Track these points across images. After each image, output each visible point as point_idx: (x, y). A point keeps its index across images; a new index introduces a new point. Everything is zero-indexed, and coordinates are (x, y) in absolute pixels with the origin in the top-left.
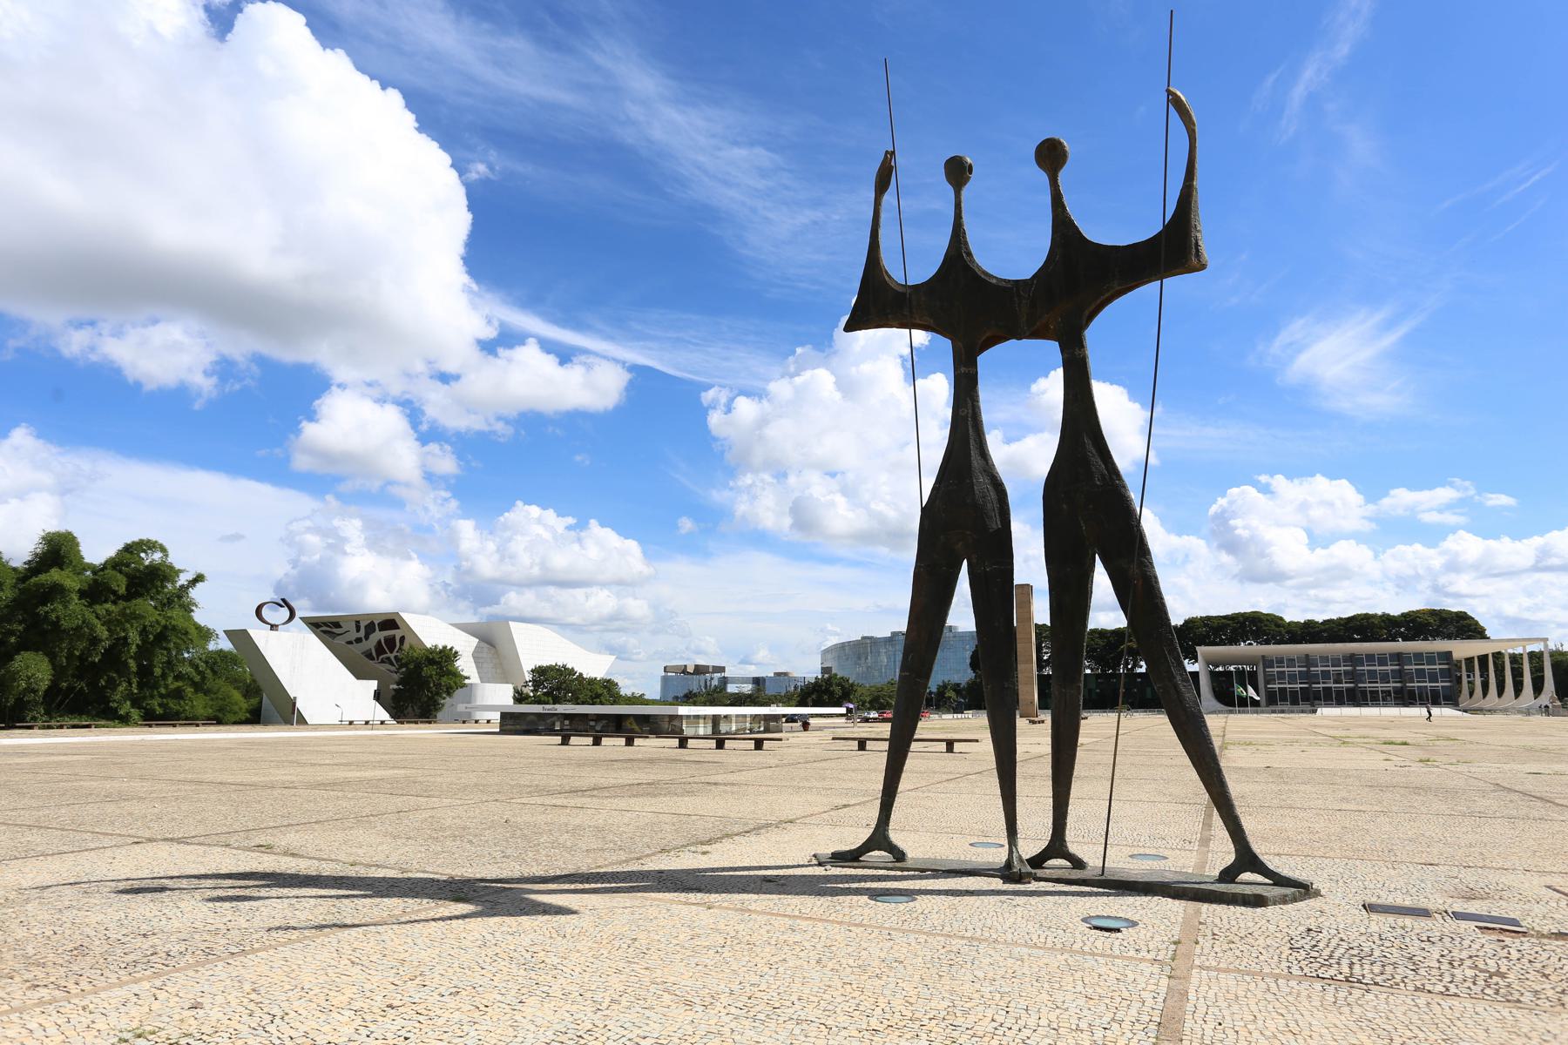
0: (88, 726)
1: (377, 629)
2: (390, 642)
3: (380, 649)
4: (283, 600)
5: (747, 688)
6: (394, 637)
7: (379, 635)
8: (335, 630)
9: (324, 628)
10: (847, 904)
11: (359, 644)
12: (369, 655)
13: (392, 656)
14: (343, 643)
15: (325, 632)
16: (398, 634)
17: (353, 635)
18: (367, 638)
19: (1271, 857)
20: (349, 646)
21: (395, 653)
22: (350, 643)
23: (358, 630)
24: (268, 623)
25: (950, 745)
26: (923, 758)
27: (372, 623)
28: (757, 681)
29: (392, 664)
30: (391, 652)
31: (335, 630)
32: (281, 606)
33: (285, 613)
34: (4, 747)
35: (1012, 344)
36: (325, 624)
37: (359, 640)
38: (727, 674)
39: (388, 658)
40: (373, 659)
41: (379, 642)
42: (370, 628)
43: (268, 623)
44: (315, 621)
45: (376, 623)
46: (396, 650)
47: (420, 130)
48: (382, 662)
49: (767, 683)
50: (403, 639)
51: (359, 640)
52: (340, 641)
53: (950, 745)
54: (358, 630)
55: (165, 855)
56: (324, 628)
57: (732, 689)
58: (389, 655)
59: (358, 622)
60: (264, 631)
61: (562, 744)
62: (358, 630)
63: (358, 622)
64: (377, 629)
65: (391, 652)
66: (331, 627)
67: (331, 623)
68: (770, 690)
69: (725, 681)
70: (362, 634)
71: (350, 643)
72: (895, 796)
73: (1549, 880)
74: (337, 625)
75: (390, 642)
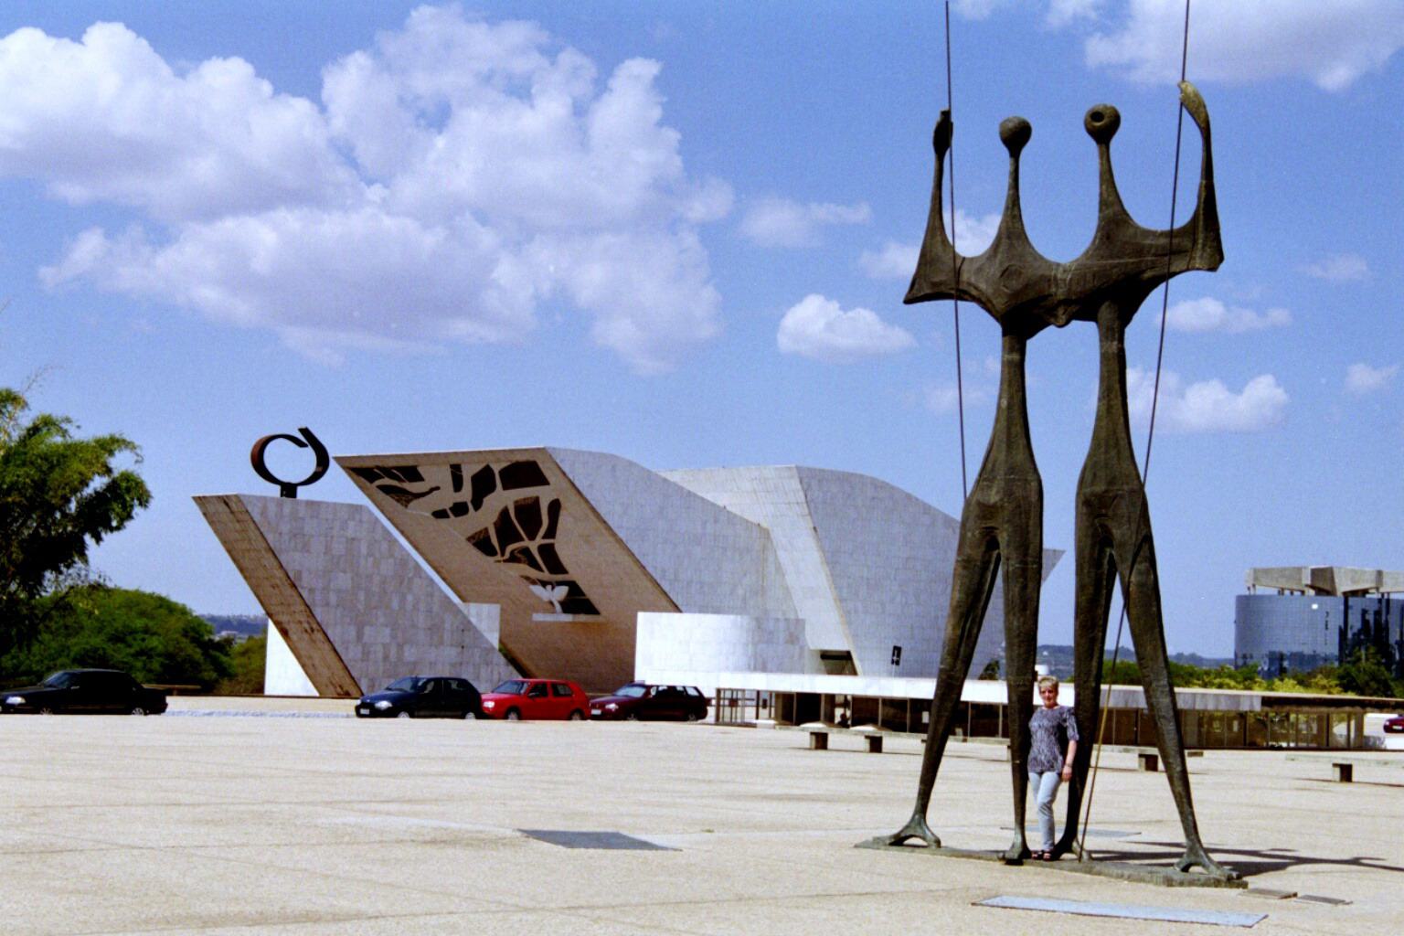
2: (528, 512)
3: (504, 527)
4: (305, 432)
6: (537, 500)
7: (503, 499)
13: (533, 546)
14: (428, 514)
15: (386, 490)
16: (545, 495)
17: (447, 498)
18: (477, 503)
21: (539, 540)
22: (440, 514)
27: (487, 471)
29: (534, 564)
33: (308, 458)
36: (387, 472)
37: (460, 509)
39: (526, 551)
41: (505, 512)
42: (484, 483)
45: (496, 468)
48: (513, 559)
50: (555, 507)
51: (460, 509)
54: (458, 485)
58: (526, 543)
65: (532, 537)
67: (397, 468)
70: (466, 494)
71: (440, 514)
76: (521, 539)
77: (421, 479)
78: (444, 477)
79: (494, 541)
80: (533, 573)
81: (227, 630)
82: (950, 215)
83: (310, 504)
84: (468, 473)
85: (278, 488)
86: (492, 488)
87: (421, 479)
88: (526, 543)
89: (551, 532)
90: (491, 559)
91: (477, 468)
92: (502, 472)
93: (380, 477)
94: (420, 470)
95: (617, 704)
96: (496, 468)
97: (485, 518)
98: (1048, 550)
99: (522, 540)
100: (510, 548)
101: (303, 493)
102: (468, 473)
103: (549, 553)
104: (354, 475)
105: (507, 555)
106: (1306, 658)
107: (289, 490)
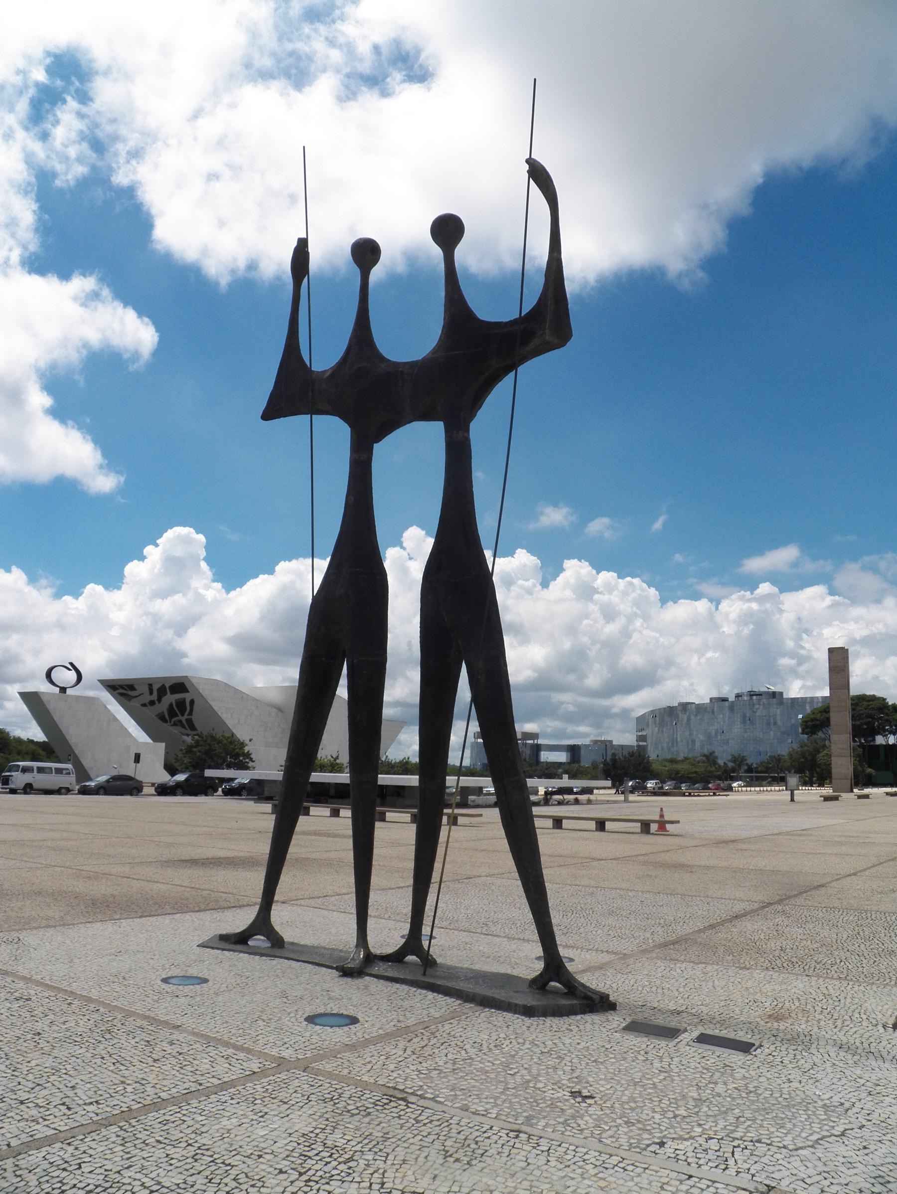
1: (168, 691)
2: (181, 704)
3: (172, 712)
4: (71, 664)
5: (562, 757)
6: (185, 699)
7: (170, 699)
10: (607, 986)
11: (152, 707)
12: (162, 718)
13: (183, 719)
14: (139, 705)
15: (122, 694)
16: (187, 697)
17: (147, 698)
18: (159, 700)
20: (144, 708)
21: (186, 717)
22: (144, 705)
24: (57, 686)
25: (645, 827)
27: (163, 687)
28: (574, 751)
29: (183, 727)
32: (70, 670)
33: (72, 675)
35: (337, 418)
36: (121, 687)
37: (152, 703)
38: (540, 741)
39: (180, 721)
40: (165, 721)
41: (171, 705)
42: (162, 691)
43: (57, 686)
44: (112, 684)
45: (167, 686)
47: (528, 172)
48: (175, 724)
49: (583, 752)
50: (192, 702)
51: (152, 703)
52: (135, 703)
53: (601, 825)
54: (151, 693)
57: (546, 757)
58: (180, 718)
61: (332, 816)
63: (150, 685)
64: (168, 691)
65: (183, 715)
67: (126, 685)
68: (586, 762)
69: (537, 748)
70: (155, 697)
71: (144, 705)
72: (429, 887)
73: (354, 1033)
75: (181, 704)
76: (177, 716)
77: (135, 690)
78: (146, 689)
79: (167, 717)
80: (183, 730)
81: (74, 767)
82: (405, 903)
83: (78, 698)
84: (155, 688)
85: (58, 689)
86: (166, 694)
87: (135, 690)
88: (180, 718)
89: (191, 713)
90: (165, 725)
91: (159, 685)
92: (170, 687)
93: (118, 689)
94: (135, 686)
95: (646, 788)
96: (167, 686)
97: (163, 706)
98: (431, 537)
99: (178, 716)
100: (173, 720)
101: (69, 691)
102: (155, 688)
103: (190, 723)
104: (110, 690)
105: (172, 723)
106: (808, 700)
107: (63, 690)
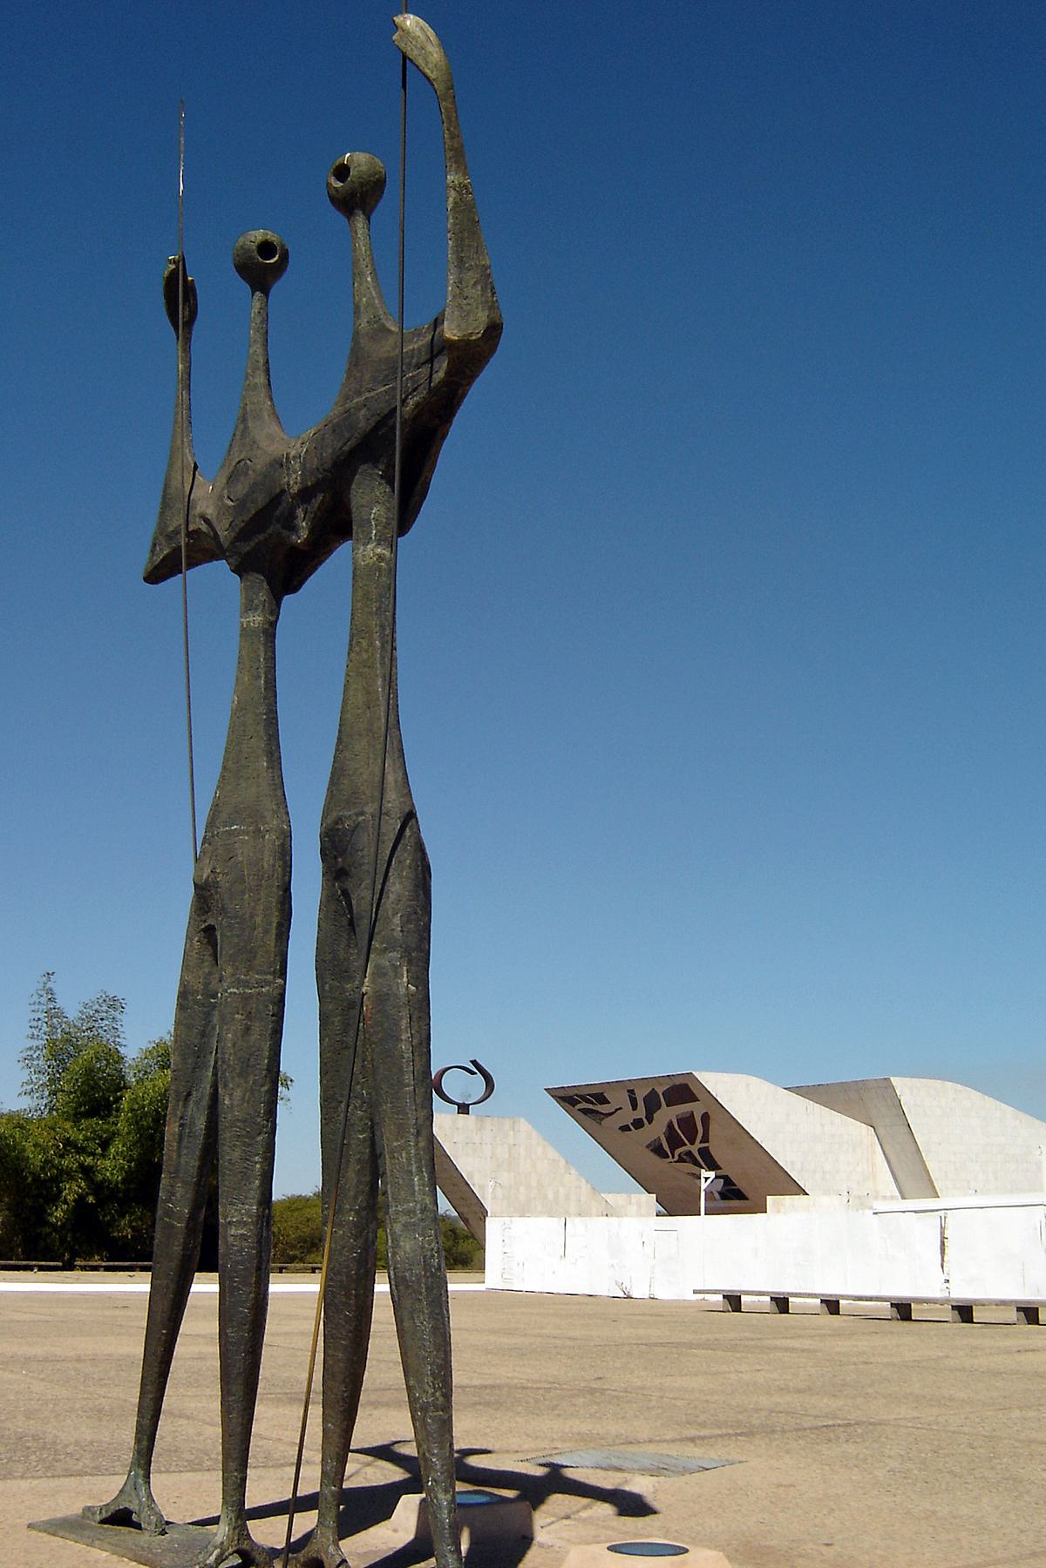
0: (30, 1268)
2: (687, 1122)
4: (474, 1063)
6: (692, 1115)
7: (668, 1114)
8: (599, 1108)
9: (584, 1105)
12: (658, 1150)
13: (694, 1149)
16: (697, 1109)
17: (628, 1116)
19: (391, 1473)
21: (698, 1145)
22: (625, 1128)
23: (634, 1107)
24: (454, 1103)
26: (1001, 1328)
30: (692, 1143)
31: (599, 1108)
34: (3, 1289)
37: (638, 1124)
39: (689, 1153)
41: (670, 1126)
42: (652, 1104)
43: (454, 1103)
46: (698, 1140)
48: (681, 1160)
50: (706, 1118)
51: (638, 1124)
55: (832, 1519)
56: (584, 1105)
58: (688, 1147)
59: (631, 1092)
60: (449, 1116)
62: (634, 1107)
63: (631, 1092)
65: (692, 1143)
66: (592, 1103)
70: (641, 1113)
71: (625, 1128)
74: (601, 1099)
